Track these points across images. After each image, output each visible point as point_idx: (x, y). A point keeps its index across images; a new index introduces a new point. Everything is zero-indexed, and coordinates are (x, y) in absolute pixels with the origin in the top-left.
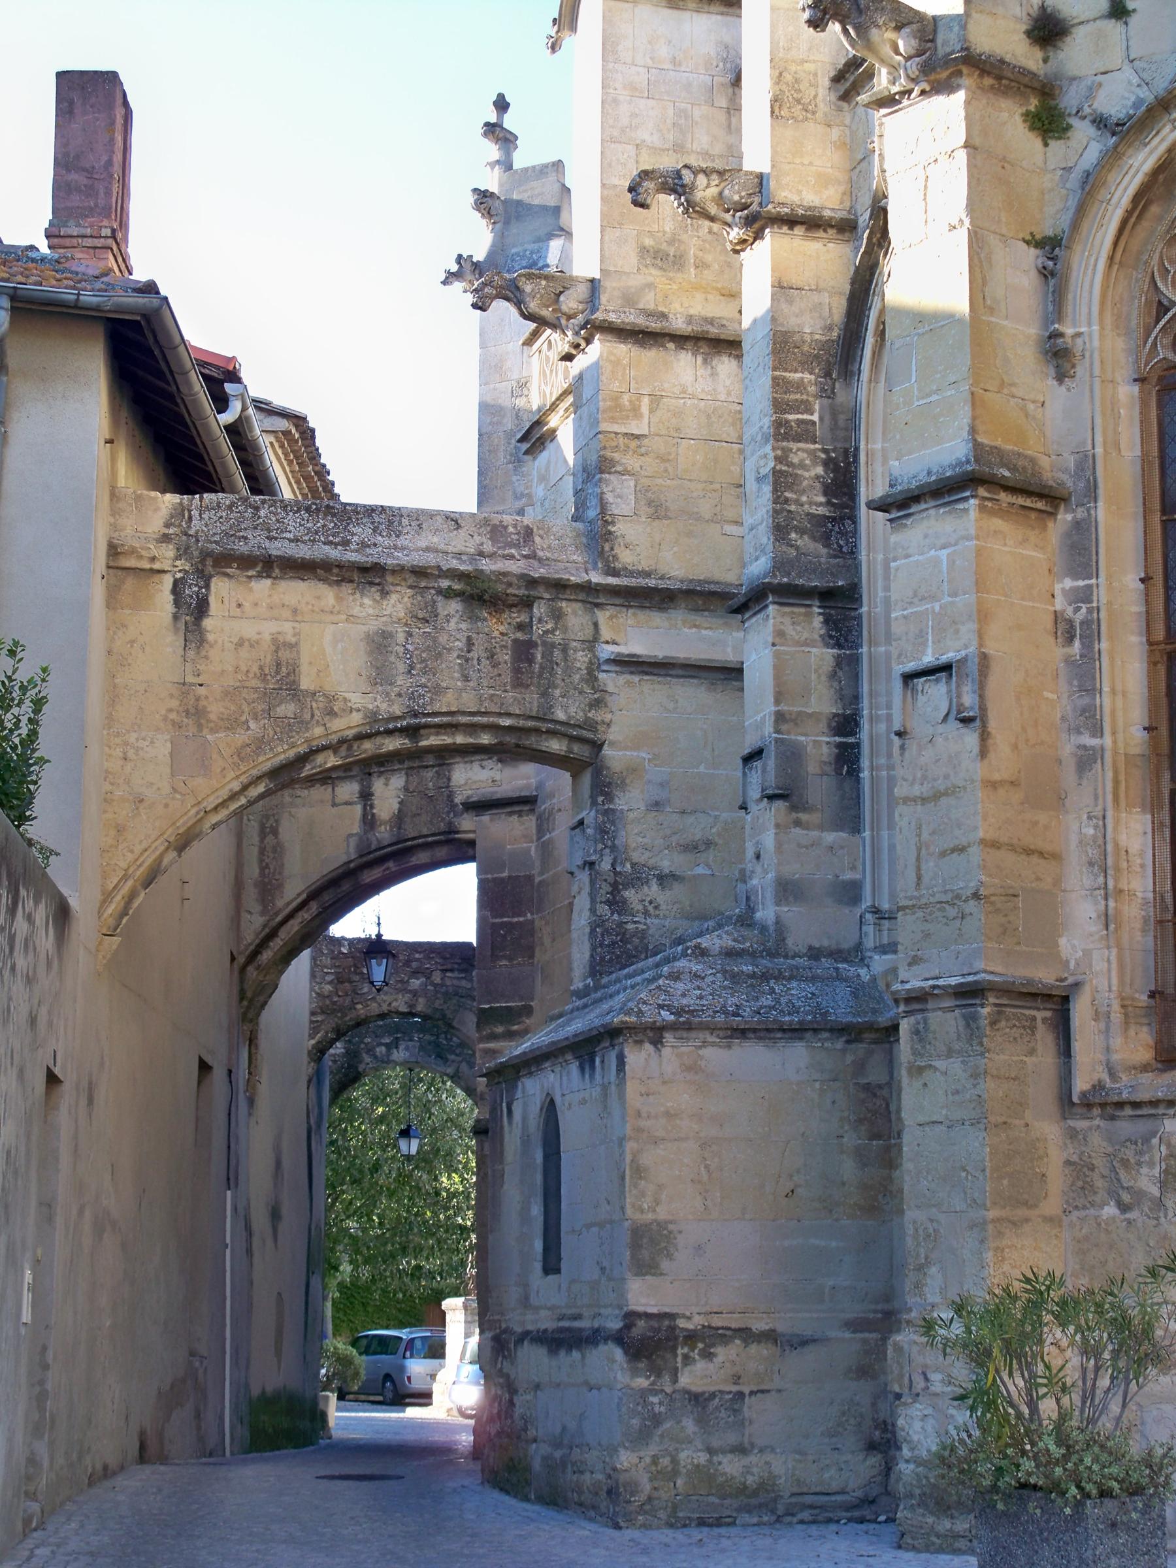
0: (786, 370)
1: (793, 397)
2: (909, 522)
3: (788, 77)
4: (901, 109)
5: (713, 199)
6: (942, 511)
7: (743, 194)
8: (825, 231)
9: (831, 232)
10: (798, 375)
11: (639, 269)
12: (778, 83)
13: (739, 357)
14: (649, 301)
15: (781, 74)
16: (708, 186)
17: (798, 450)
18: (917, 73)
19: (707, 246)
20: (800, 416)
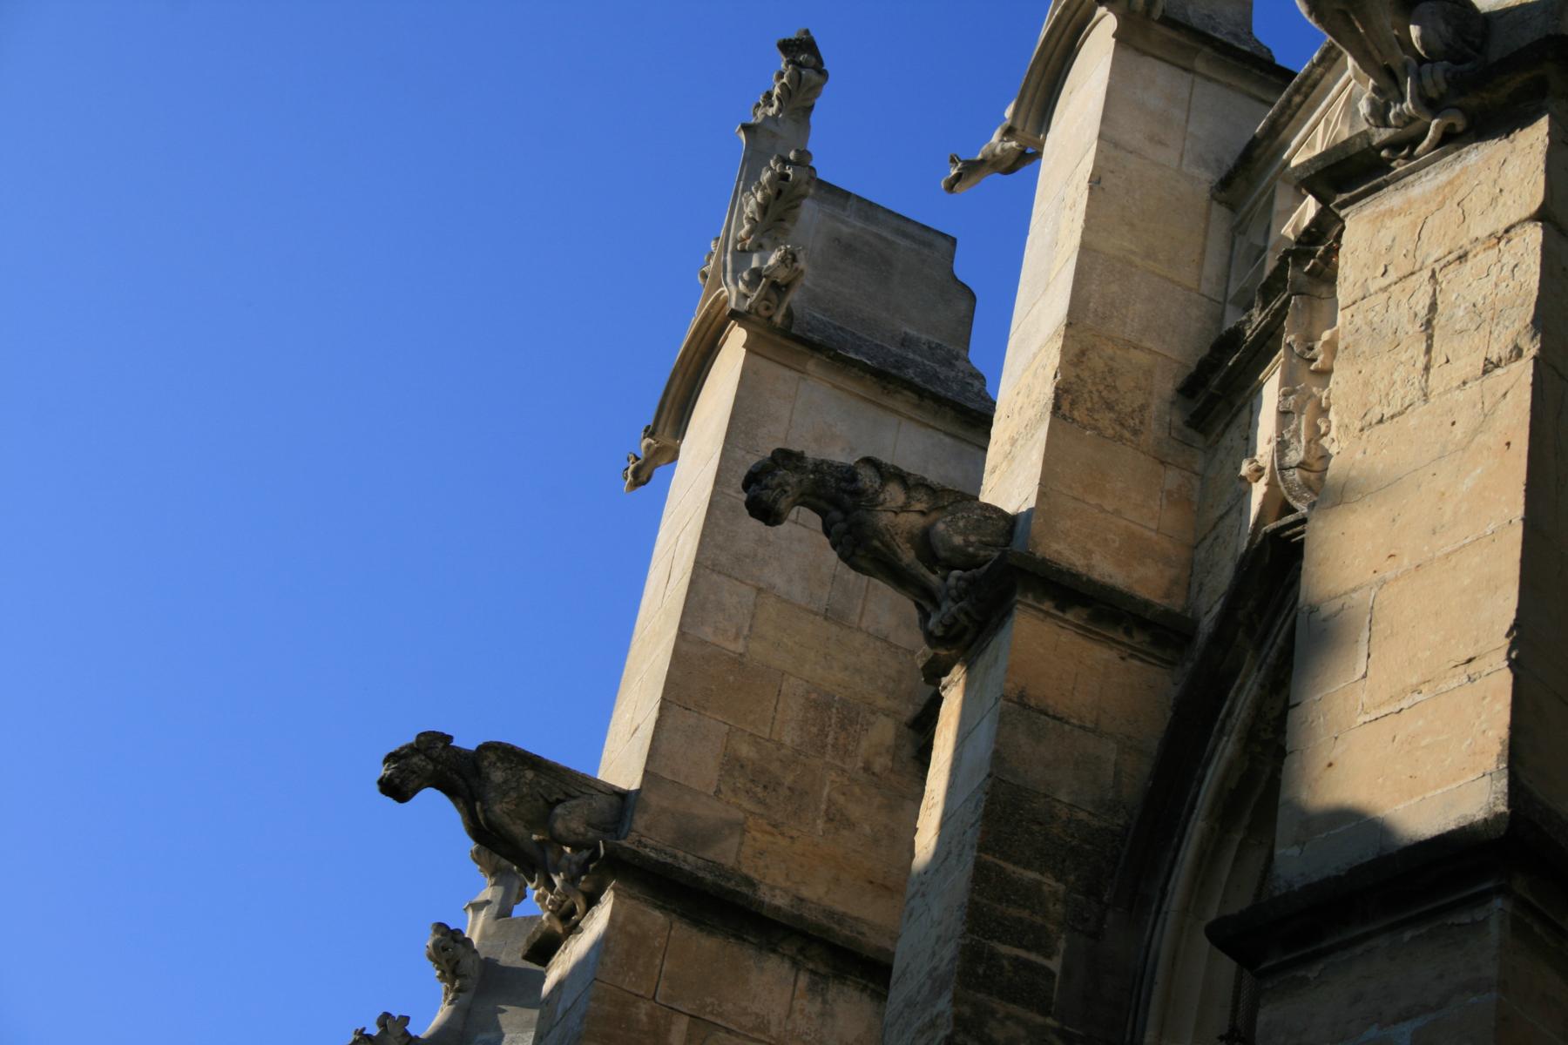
0: (1007, 858)
1: (1013, 912)
2: (1312, 973)
3: (1097, 363)
4: (1387, 183)
5: (911, 538)
6: (1407, 935)
7: (972, 539)
8: (1128, 632)
9: (1140, 638)
10: (1031, 875)
11: (718, 791)
12: (1075, 365)
13: (880, 996)
14: (726, 853)
15: (1083, 353)
16: (904, 509)
17: (1008, 1017)
18: (1443, 87)
19: (857, 790)
20: (1023, 953)
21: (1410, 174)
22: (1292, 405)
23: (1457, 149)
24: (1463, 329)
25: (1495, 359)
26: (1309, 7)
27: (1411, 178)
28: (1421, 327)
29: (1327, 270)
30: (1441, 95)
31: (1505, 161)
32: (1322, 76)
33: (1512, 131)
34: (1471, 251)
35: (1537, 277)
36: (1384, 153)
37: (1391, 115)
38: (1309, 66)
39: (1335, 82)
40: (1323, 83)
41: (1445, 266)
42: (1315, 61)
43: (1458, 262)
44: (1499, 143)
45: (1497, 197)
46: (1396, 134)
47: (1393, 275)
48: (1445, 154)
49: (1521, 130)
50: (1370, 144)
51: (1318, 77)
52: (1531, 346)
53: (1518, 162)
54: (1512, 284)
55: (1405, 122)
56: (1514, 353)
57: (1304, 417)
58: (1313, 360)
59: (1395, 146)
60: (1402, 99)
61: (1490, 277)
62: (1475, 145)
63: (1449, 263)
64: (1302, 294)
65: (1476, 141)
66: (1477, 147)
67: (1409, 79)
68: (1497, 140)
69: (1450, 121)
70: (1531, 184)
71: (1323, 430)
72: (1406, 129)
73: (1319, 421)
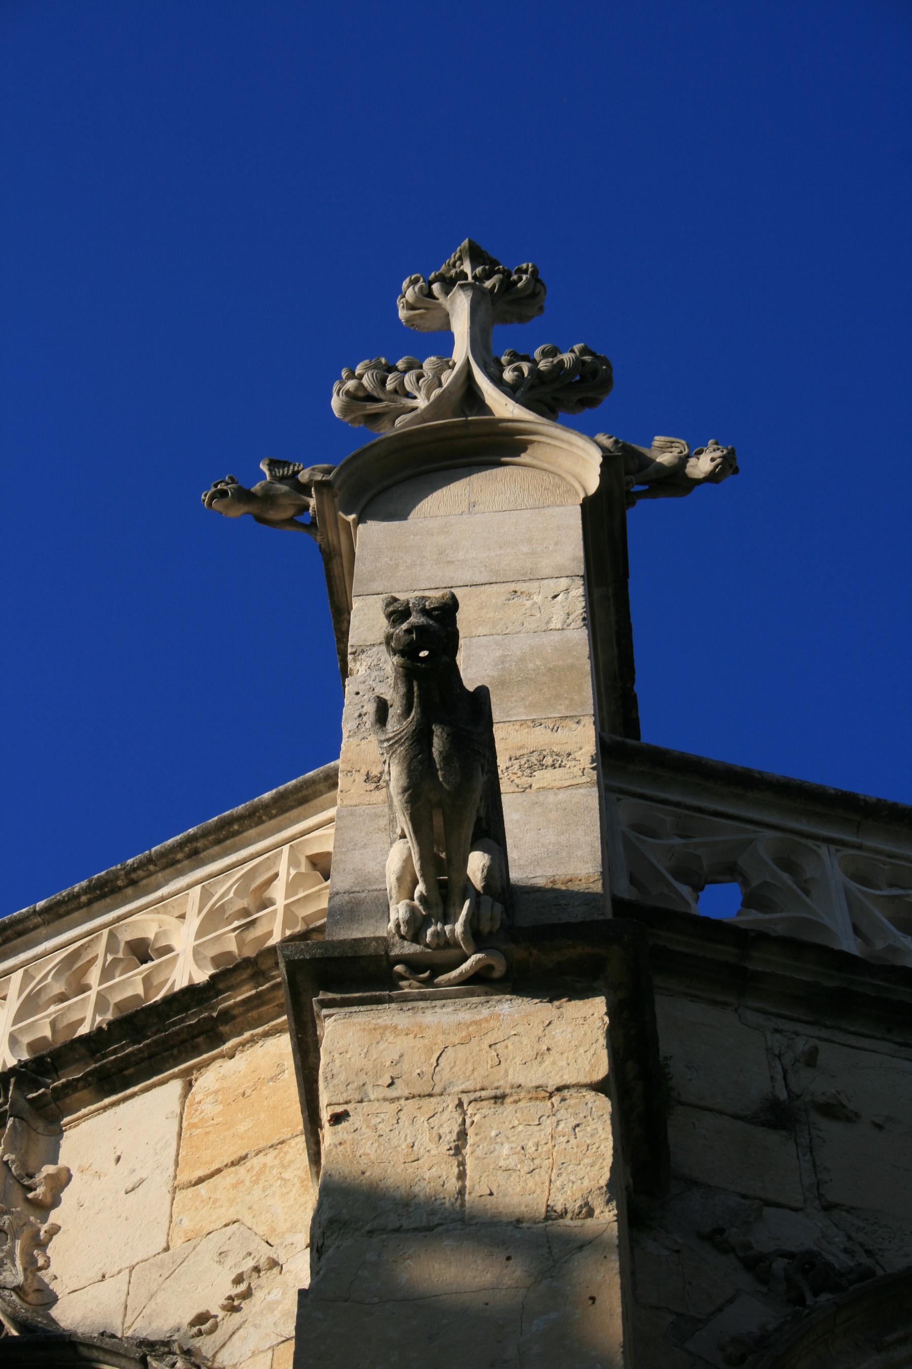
4: (391, 1000)
21: (421, 1000)
22: (6, 1225)
23: (486, 994)
24: (510, 1167)
25: (559, 1208)
26: (409, 783)
27: (421, 1004)
28: (448, 1150)
29: (53, 1105)
30: (491, 933)
31: (550, 1023)
32: (36, 927)
33: (558, 998)
34: (511, 1095)
35: (610, 1143)
36: (399, 968)
37: (430, 931)
38: (28, 911)
39: (48, 938)
40: (33, 934)
41: (475, 1100)
42: (37, 909)
43: (492, 1101)
44: (540, 1004)
45: (543, 1054)
46: (422, 953)
47: (401, 1089)
48: (472, 995)
49: (569, 1000)
50: (387, 953)
51: (31, 926)
52: (607, 1210)
53: (569, 1029)
54: (573, 1141)
55: (438, 944)
56: (584, 1210)
57: (18, 1243)
58: (31, 1189)
59: (414, 966)
60: (447, 918)
61: (542, 1127)
62: (508, 997)
63: (481, 1099)
64: (22, 1119)
65: (512, 993)
66: (511, 1000)
67: (467, 903)
68: (536, 1001)
69: (492, 962)
70: (589, 1054)
71: (41, 1262)
72: (436, 952)
73: (35, 1252)
